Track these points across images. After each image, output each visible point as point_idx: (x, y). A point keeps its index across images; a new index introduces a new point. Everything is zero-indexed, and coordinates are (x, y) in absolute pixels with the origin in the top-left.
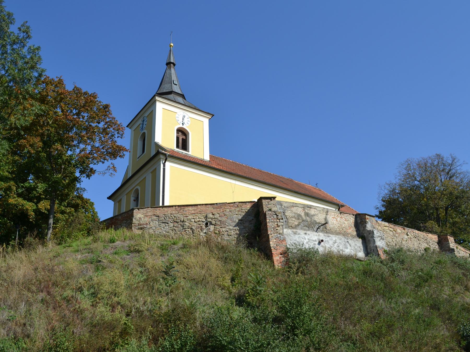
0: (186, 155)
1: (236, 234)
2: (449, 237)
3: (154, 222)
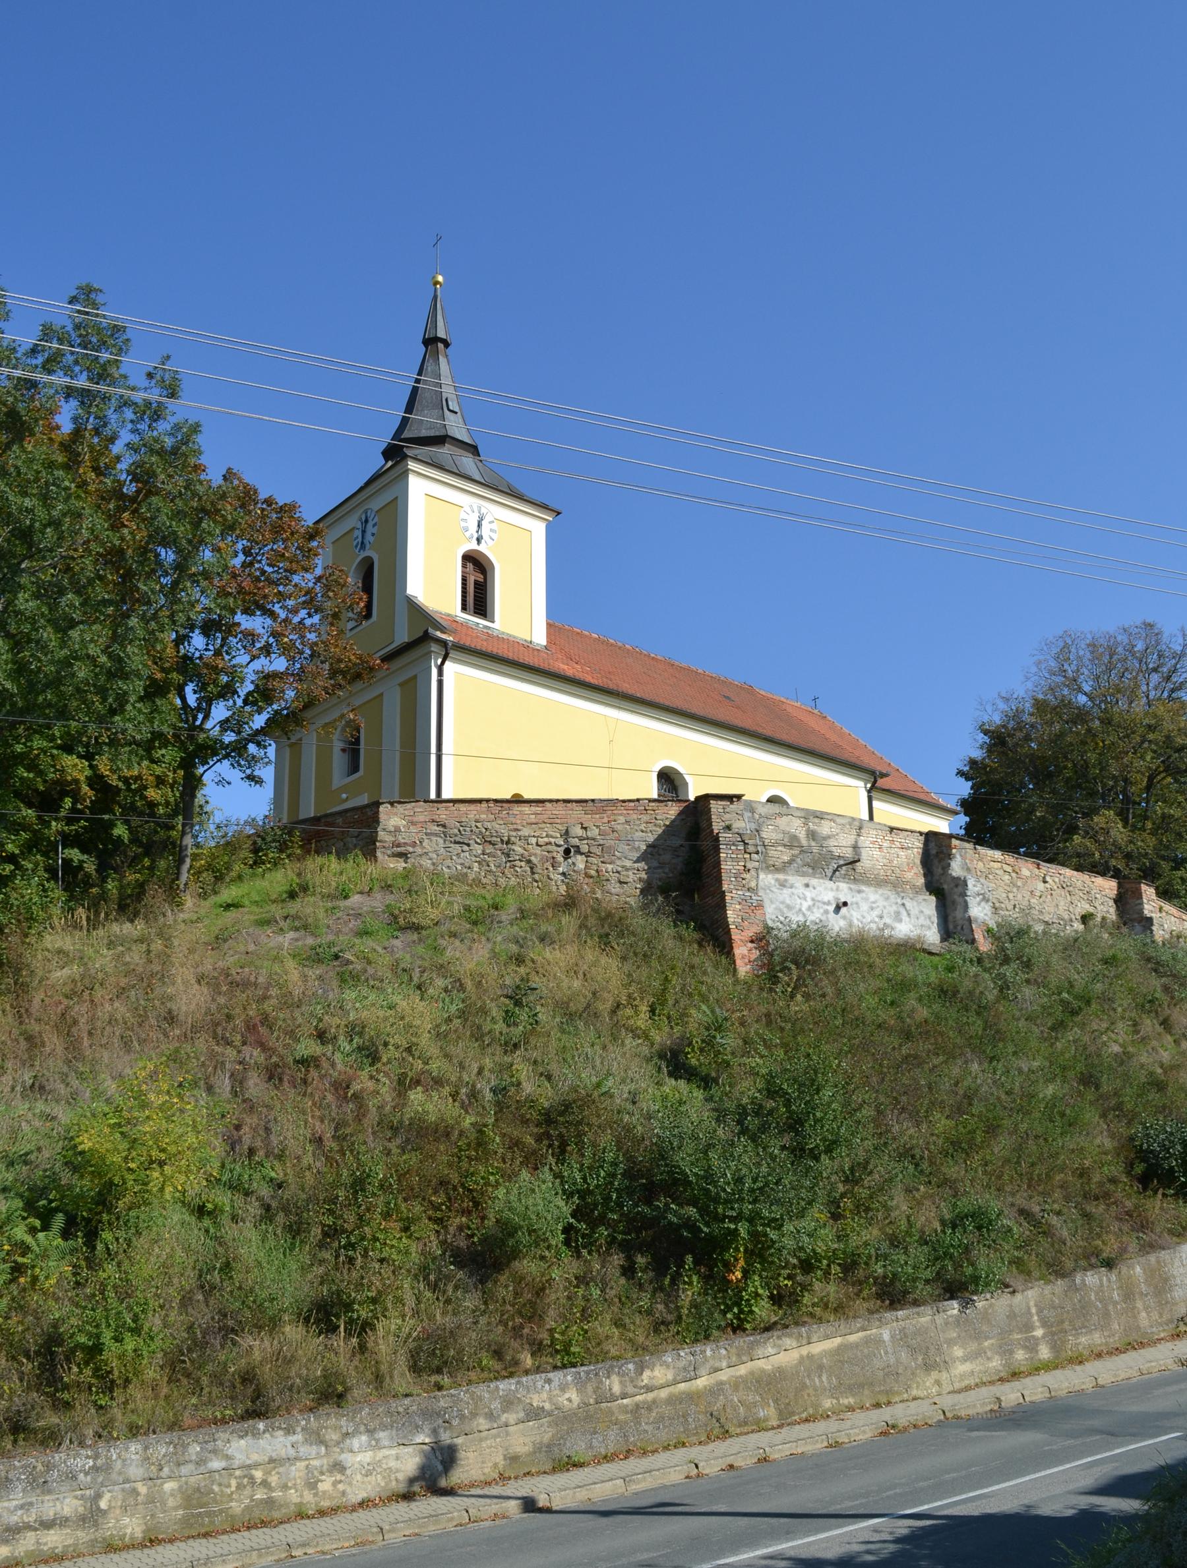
0: (490, 636)
1: (640, 880)
2: (1143, 887)
3: (434, 839)
